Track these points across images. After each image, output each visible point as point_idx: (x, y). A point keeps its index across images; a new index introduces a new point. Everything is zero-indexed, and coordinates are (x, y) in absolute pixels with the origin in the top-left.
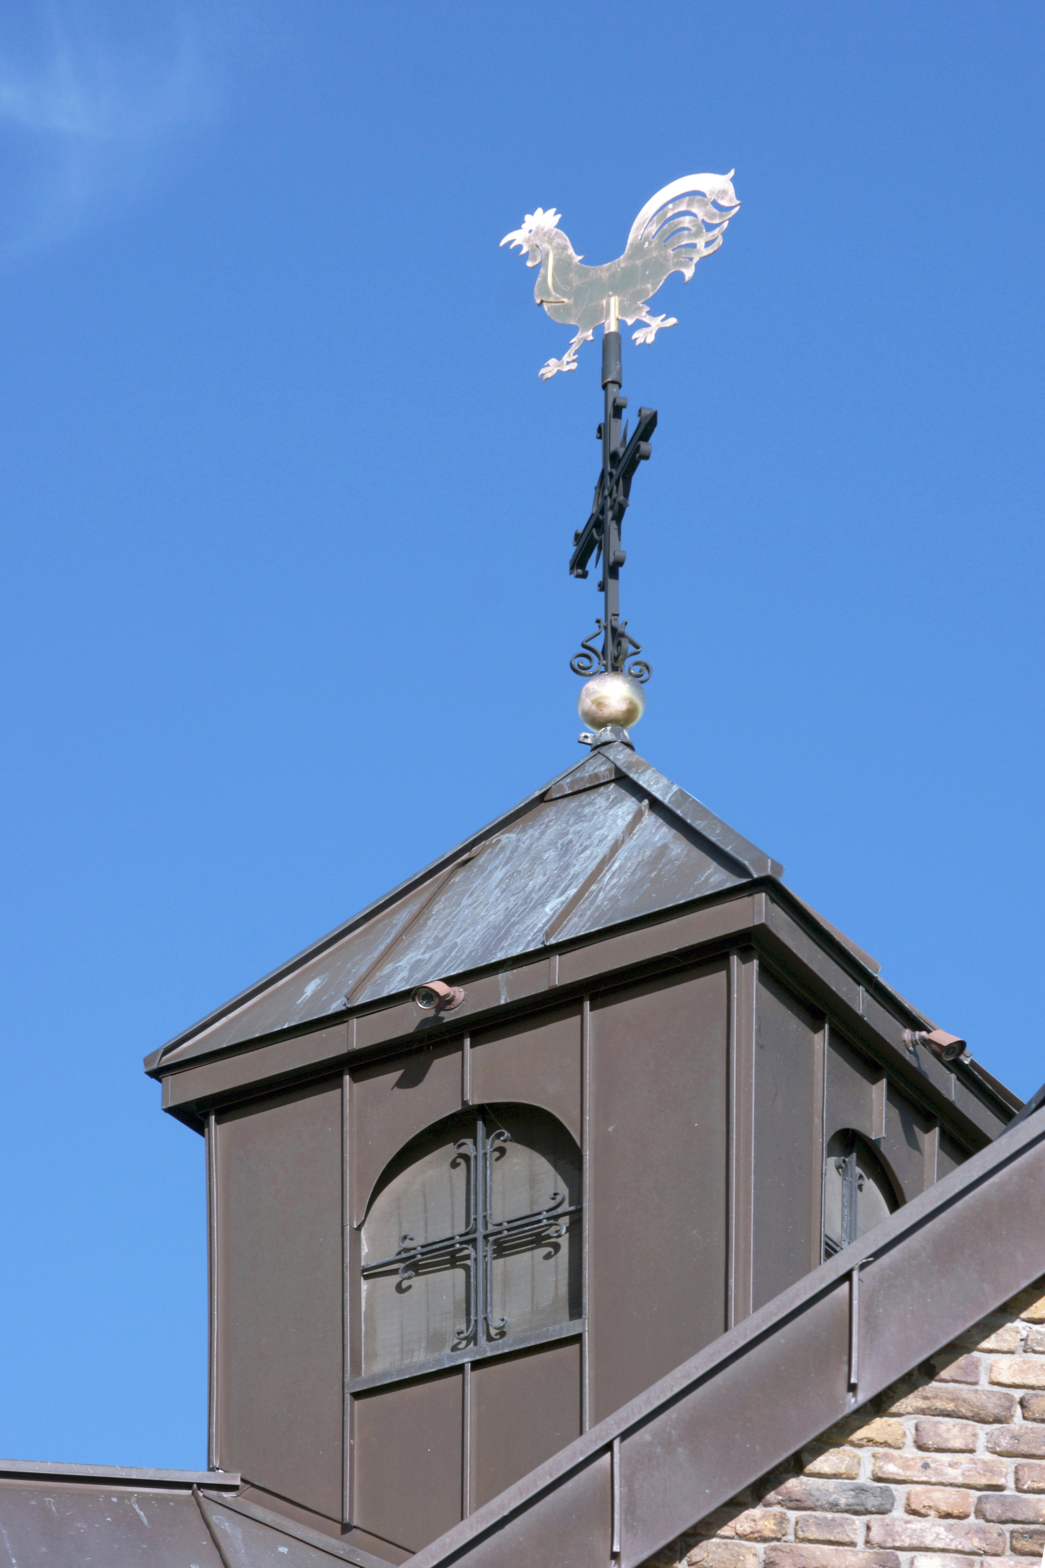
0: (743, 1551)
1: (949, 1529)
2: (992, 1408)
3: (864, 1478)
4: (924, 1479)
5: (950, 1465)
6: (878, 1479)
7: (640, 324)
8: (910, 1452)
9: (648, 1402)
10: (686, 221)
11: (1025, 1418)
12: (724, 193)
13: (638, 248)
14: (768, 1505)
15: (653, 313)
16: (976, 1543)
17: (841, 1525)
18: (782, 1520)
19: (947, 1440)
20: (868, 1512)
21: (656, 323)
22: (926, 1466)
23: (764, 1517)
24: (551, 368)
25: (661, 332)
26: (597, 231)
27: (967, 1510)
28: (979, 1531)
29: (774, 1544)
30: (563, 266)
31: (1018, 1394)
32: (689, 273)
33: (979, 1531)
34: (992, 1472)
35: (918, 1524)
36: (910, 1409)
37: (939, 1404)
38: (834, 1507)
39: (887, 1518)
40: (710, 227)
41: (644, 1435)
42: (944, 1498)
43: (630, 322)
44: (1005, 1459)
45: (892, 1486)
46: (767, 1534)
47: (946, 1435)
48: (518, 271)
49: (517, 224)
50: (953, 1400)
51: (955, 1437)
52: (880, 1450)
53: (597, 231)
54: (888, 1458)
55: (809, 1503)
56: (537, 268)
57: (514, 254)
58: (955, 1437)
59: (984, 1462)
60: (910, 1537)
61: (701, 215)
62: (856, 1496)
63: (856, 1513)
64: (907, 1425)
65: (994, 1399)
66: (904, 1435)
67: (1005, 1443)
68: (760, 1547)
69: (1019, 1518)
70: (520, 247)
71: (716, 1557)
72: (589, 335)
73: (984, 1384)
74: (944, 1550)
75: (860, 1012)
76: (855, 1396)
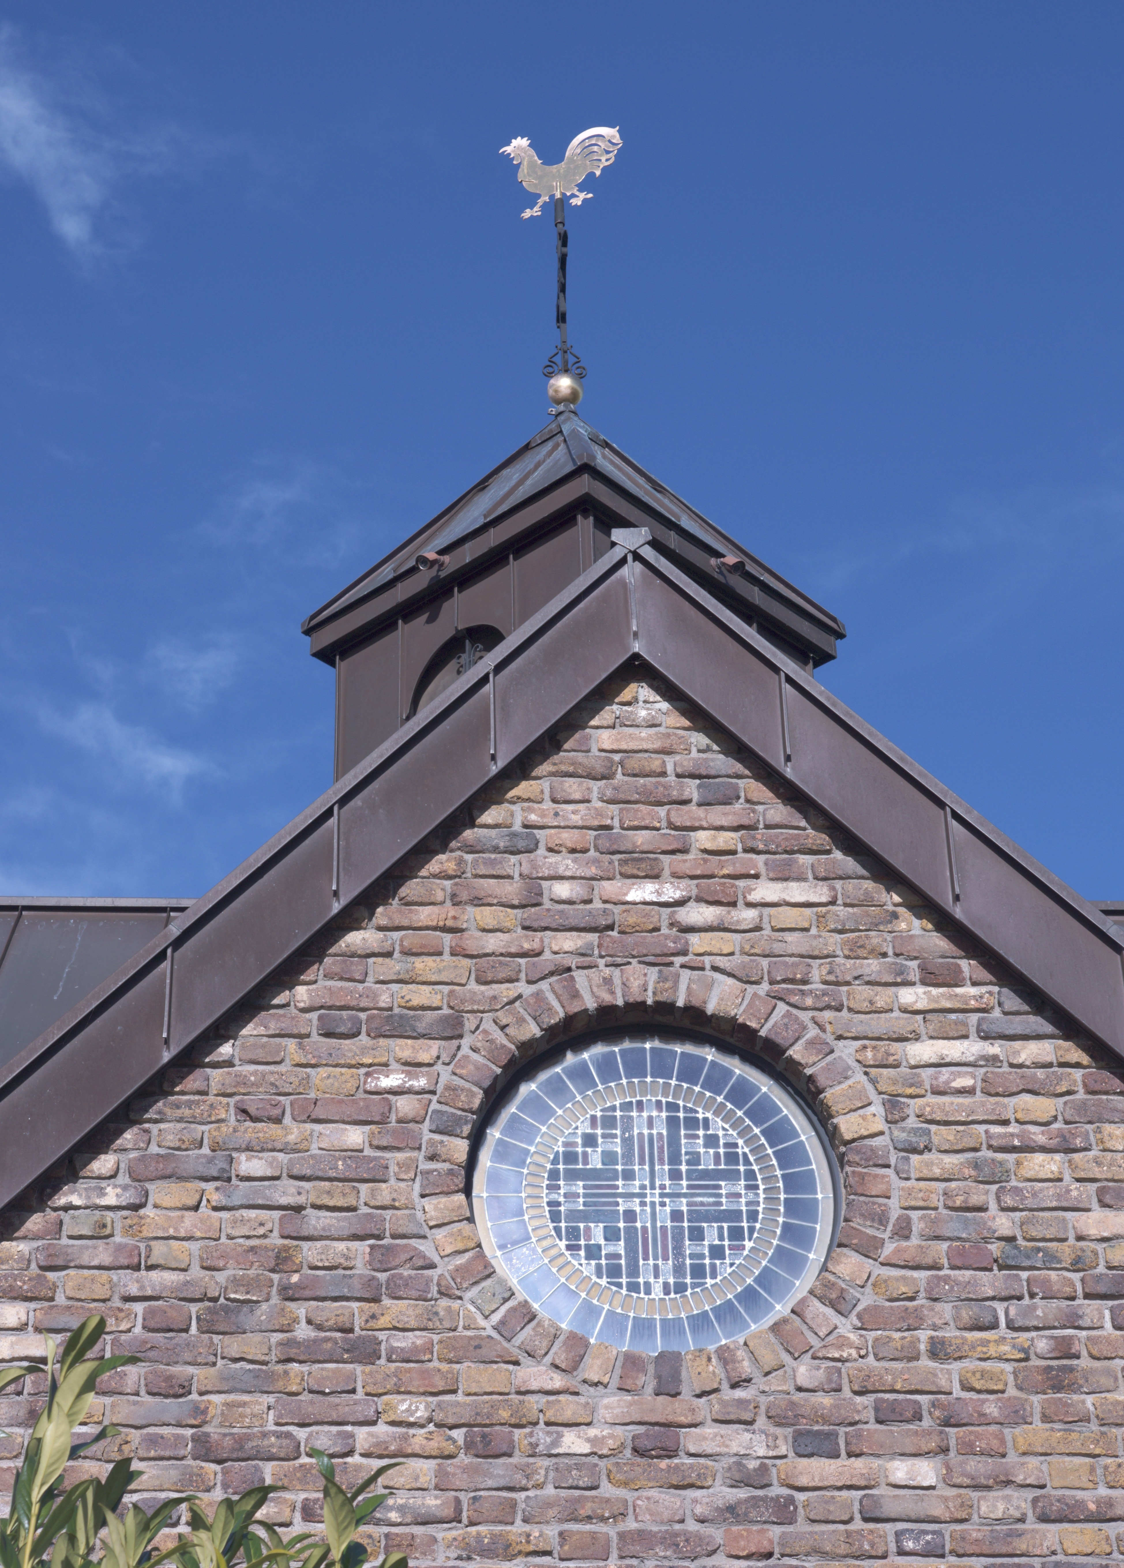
0: (434, 887)
1: (575, 861)
2: (599, 769)
3: (517, 827)
4: (556, 824)
5: (573, 813)
6: (526, 826)
7: (574, 196)
8: (548, 805)
9: (355, 777)
10: (595, 148)
11: (624, 775)
12: (614, 137)
13: (571, 160)
14: (452, 851)
15: (580, 191)
16: (593, 871)
17: (501, 863)
18: (460, 862)
19: (570, 794)
20: (519, 852)
21: (582, 196)
22: (556, 814)
23: (448, 860)
24: (527, 214)
25: (585, 200)
26: (551, 151)
27: (587, 845)
28: (596, 861)
29: (457, 880)
30: (532, 164)
31: (617, 757)
32: (598, 173)
33: (596, 861)
34: (601, 815)
35: (553, 859)
36: (545, 773)
37: (563, 768)
38: (495, 849)
39: (532, 856)
40: (608, 152)
41: (357, 802)
42: (569, 838)
43: (568, 194)
44: (611, 806)
45: (535, 831)
46: (451, 872)
47: (569, 790)
48: (510, 166)
49: (508, 143)
50: (572, 764)
51: (575, 791)
52: (526, 804)
53: (551, 151)
54: (530, 810)
55: (479, 848)
56: (520, 164)
57: (507, 157)
58: (575, 791)
59: (596, 809)
60: (548, 869)
61: (603, 146)
62: (510, 840)
63: (512, 853)
64: (545, 784)
65: (600, 762)
66: (542, 792)
67: (609, 793)
68: (448, 883)
69: (622, 849)
70: (509, 154)
71: (416, 892)
72: (547, 199)
73: (594, 751)
74: (573, 878)
75: (672, 547)
76: (496, 763)
